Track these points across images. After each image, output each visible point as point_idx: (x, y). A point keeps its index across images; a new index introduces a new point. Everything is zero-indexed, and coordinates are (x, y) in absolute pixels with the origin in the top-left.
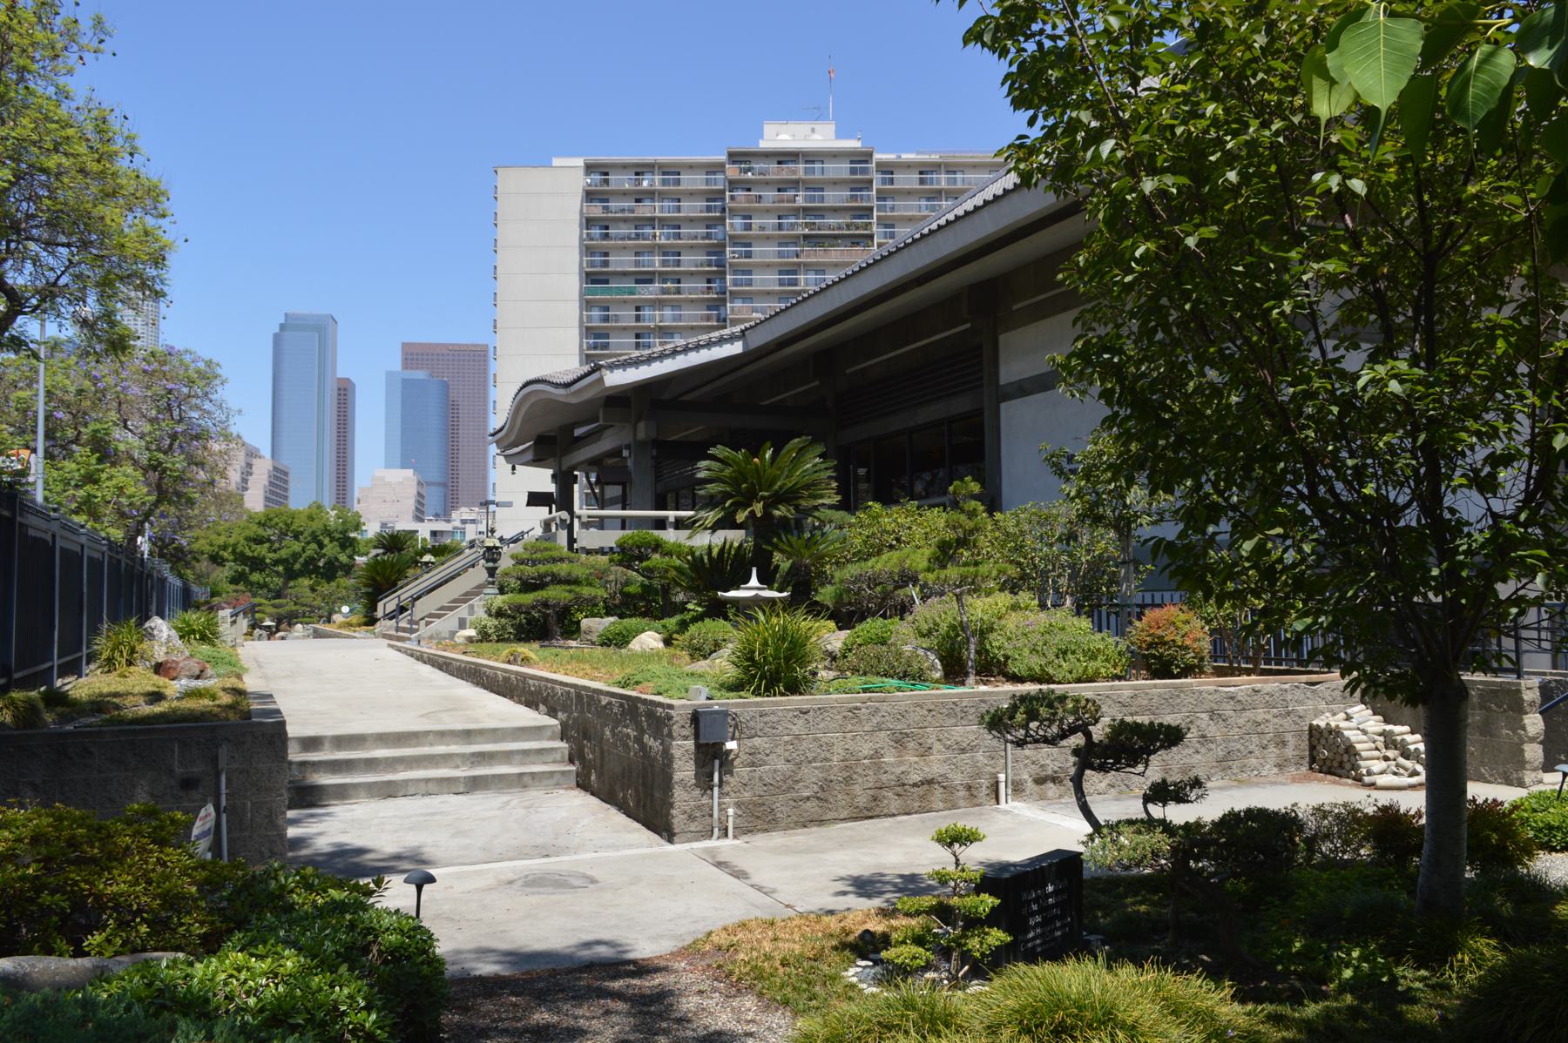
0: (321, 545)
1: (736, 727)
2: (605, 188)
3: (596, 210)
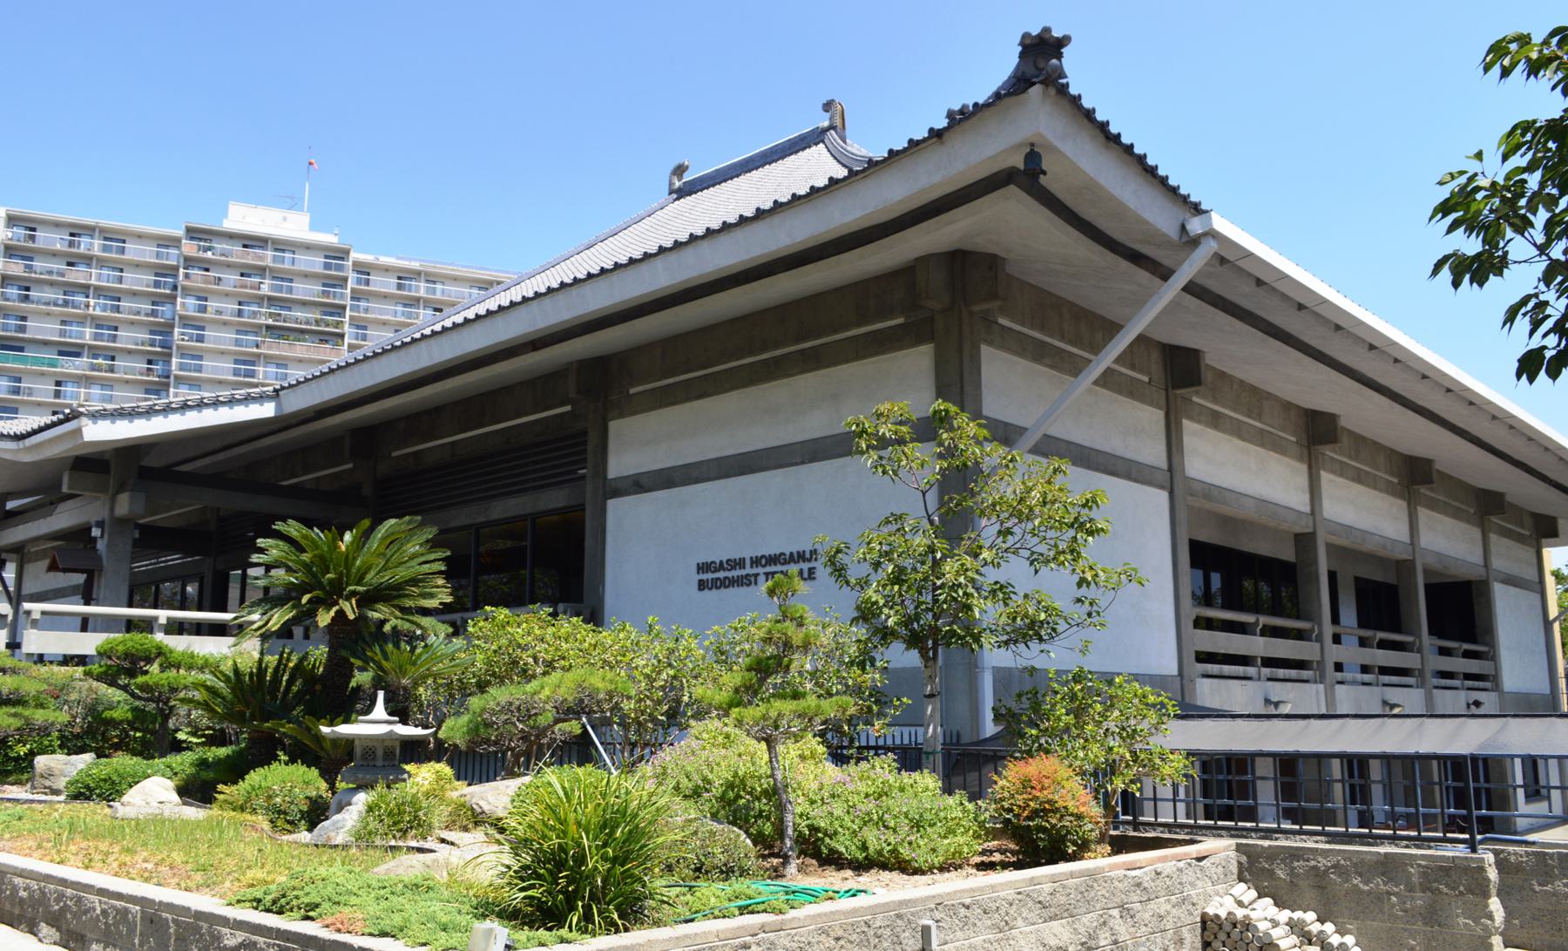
2: (30, 244)
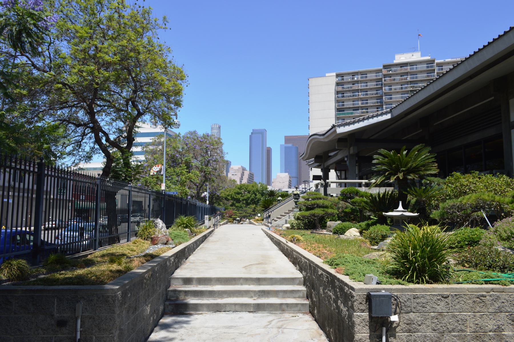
0: (256, 195)
1: (397, 305)
3: (340, 88)
